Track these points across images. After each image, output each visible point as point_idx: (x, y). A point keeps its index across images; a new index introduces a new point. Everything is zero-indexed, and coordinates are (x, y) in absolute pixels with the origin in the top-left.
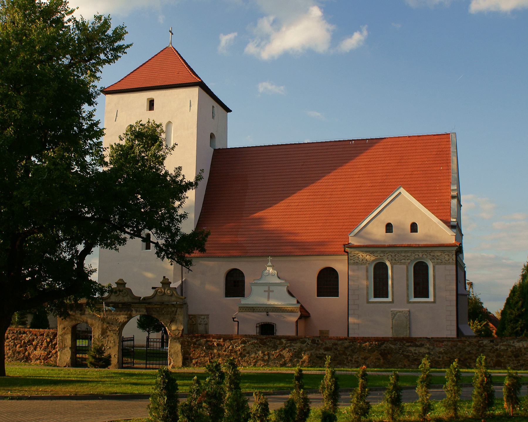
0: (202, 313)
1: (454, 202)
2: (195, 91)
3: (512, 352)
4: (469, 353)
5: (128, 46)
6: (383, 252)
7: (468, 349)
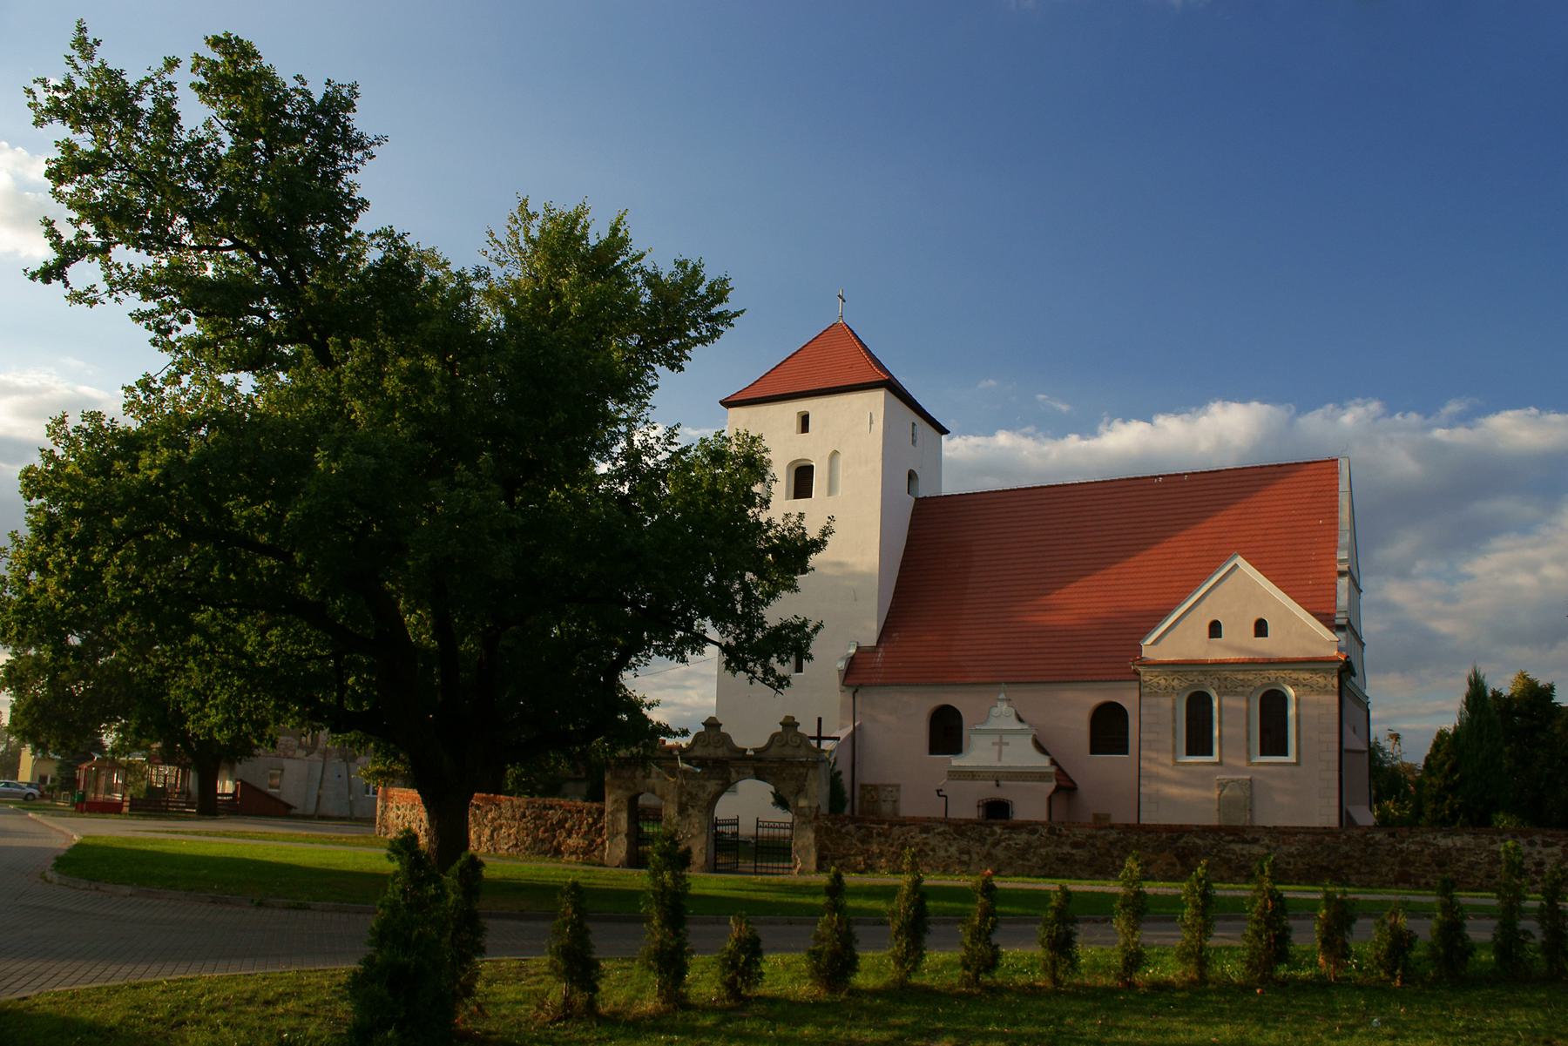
0: (887, 782)
1: (1343, 582)
2: (878, 397)
3: (1432, 855)
4: (1347, 856)
5: (736, 314)
6: (1202, 672)
7: (1345, 849)
